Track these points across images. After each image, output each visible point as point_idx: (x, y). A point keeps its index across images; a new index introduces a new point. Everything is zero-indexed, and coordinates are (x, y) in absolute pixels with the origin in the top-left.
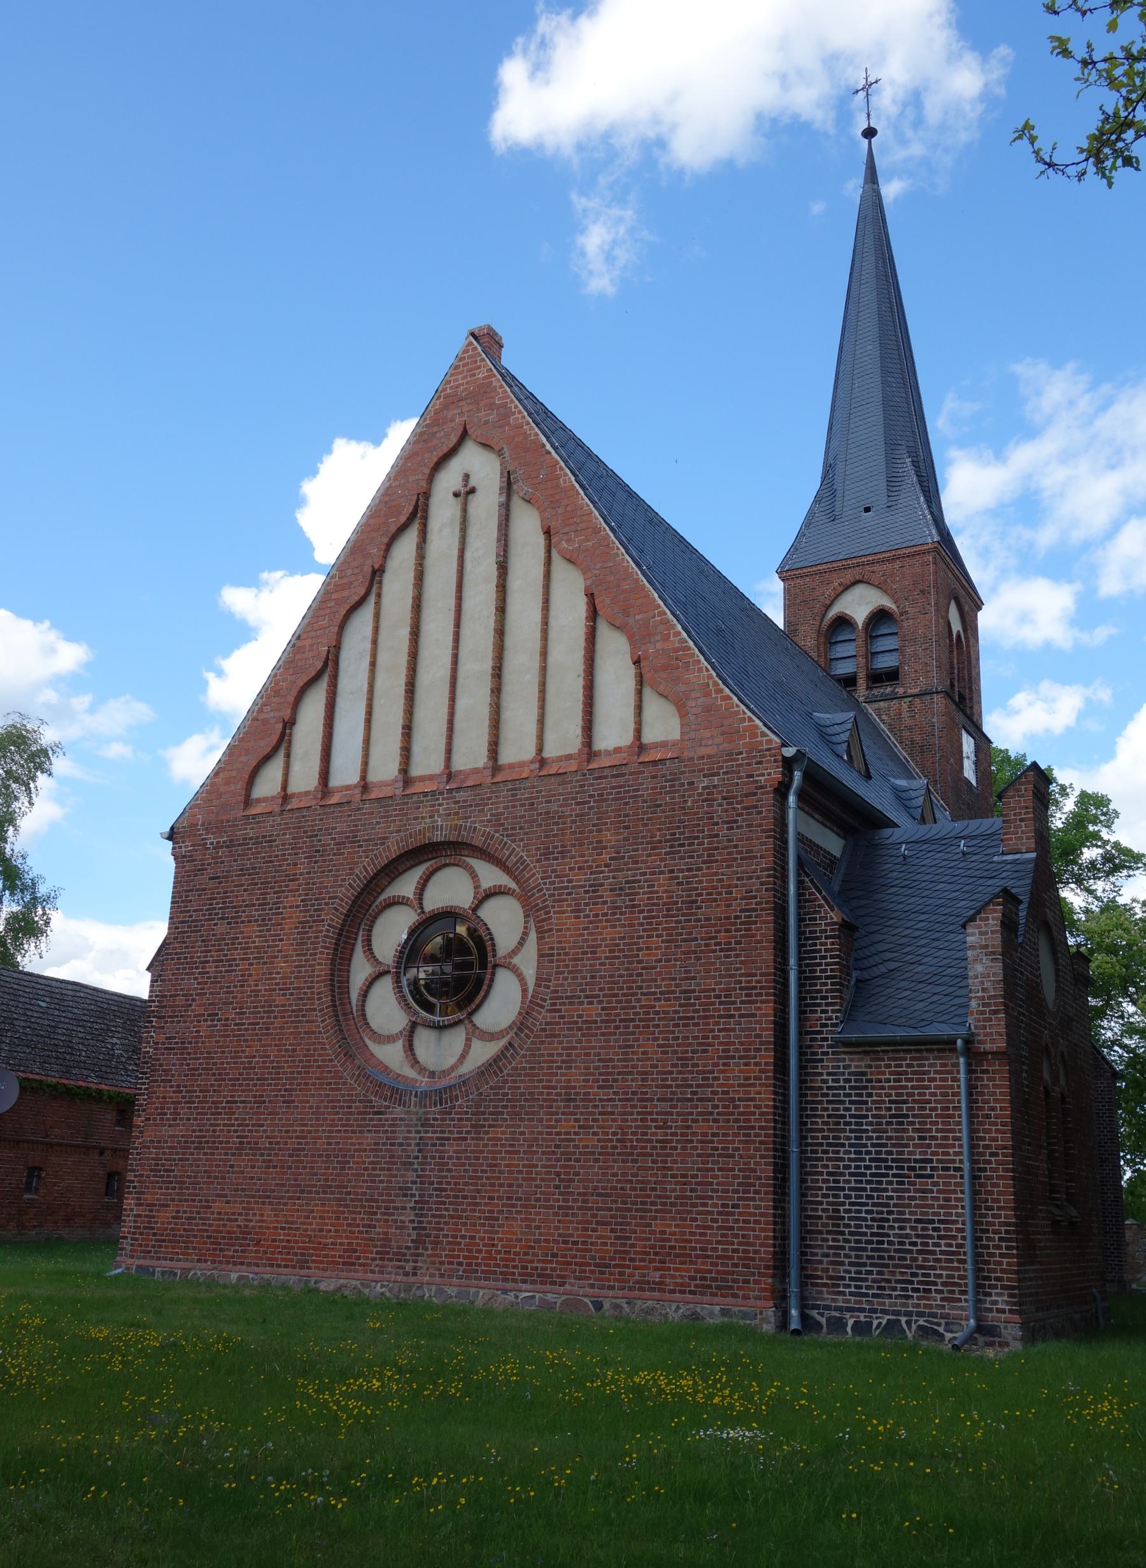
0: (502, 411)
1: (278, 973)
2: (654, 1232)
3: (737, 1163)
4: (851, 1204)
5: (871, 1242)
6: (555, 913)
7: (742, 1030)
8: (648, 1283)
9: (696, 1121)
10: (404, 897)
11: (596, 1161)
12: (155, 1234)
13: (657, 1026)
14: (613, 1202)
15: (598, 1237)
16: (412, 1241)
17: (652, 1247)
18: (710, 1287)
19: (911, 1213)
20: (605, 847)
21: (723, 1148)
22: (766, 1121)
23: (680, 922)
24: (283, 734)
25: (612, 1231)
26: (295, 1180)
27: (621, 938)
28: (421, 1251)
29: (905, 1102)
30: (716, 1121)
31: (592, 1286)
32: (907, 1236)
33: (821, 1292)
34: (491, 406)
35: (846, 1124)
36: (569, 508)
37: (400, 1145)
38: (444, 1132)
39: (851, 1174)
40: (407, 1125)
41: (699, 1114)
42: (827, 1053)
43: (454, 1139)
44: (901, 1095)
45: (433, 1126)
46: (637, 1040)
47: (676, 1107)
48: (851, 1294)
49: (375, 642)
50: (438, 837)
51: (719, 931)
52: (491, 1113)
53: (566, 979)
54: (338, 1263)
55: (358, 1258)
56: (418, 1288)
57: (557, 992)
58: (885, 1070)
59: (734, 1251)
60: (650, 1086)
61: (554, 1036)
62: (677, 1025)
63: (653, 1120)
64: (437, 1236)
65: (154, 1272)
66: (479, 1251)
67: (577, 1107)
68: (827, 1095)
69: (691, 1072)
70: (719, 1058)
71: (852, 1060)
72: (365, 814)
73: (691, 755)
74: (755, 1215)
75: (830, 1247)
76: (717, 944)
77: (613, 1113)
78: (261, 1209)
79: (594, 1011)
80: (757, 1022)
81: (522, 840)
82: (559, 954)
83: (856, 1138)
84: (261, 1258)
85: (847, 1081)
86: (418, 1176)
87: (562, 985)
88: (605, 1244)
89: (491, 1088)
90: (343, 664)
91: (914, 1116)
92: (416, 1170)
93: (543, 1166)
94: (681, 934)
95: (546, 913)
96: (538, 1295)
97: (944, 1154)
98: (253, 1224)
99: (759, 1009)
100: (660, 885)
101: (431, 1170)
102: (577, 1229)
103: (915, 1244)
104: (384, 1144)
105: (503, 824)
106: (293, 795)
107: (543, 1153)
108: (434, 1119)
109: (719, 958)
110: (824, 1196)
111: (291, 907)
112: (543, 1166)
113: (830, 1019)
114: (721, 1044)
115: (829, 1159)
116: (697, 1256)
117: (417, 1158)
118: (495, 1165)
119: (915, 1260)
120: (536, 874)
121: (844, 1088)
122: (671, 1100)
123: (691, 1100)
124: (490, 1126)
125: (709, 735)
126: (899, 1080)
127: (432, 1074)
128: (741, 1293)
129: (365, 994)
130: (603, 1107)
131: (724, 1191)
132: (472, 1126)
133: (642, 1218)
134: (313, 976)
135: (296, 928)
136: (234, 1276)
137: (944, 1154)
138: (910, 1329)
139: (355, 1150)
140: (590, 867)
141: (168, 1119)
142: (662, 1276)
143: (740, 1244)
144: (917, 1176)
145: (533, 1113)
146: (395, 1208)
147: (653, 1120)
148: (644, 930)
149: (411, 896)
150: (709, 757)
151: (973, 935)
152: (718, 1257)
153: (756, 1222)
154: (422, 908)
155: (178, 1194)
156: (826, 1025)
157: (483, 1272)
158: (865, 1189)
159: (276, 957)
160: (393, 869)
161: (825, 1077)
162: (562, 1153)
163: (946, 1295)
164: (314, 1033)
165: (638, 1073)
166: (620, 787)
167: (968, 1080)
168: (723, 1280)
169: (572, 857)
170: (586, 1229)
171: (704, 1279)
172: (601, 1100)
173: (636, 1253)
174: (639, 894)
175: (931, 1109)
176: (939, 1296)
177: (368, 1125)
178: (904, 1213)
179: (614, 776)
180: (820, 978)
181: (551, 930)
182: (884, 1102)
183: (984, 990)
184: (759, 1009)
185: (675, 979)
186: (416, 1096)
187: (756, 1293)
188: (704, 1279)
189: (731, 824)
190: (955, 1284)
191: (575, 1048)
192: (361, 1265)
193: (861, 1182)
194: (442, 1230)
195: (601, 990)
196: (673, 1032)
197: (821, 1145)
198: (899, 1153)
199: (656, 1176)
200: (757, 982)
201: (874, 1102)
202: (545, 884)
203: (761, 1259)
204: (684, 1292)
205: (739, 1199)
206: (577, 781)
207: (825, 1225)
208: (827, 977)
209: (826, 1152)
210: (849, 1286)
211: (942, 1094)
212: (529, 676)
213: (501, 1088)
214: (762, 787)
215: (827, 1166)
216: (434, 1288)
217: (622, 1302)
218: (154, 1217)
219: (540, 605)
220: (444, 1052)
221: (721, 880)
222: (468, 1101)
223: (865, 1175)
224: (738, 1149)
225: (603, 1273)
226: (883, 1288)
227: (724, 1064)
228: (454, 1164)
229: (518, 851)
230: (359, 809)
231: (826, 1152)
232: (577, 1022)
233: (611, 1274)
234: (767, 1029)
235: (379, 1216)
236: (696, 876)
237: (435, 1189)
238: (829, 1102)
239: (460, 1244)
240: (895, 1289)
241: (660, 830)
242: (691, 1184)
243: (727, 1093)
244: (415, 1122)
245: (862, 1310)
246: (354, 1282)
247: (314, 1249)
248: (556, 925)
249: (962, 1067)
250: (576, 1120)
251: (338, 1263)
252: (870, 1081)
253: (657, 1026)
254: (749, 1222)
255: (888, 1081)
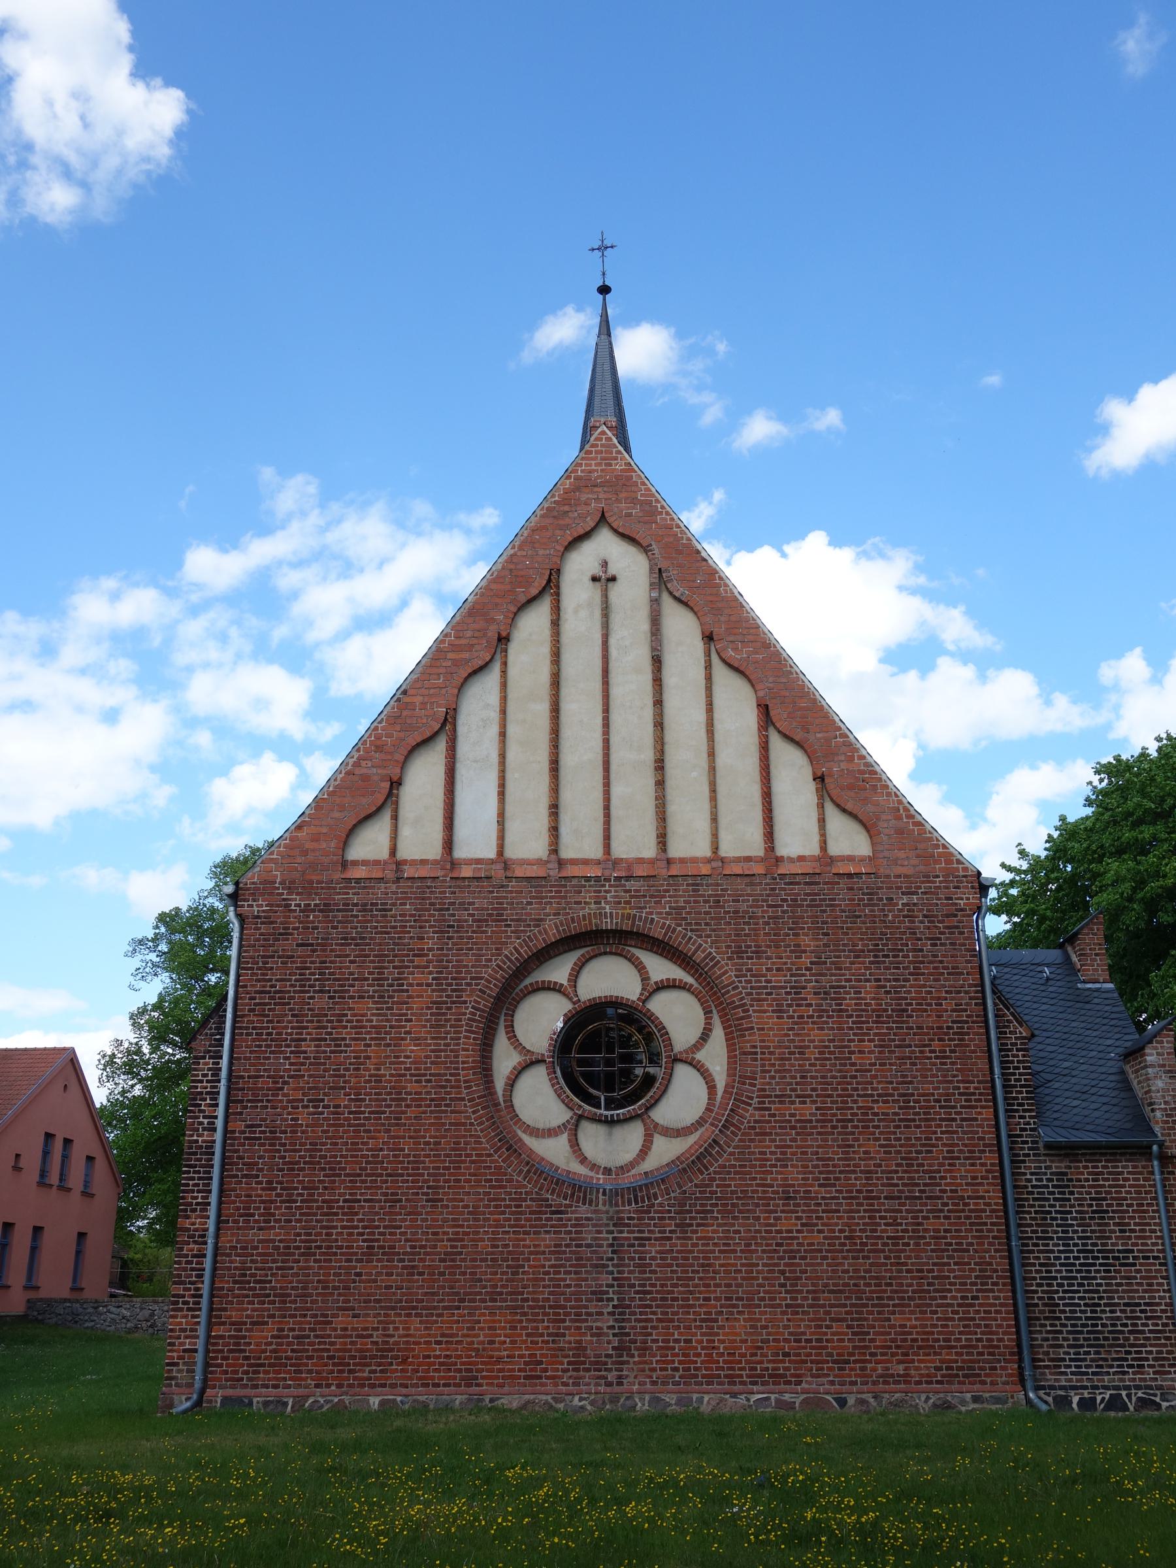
0: (647, 508)
1: (407, 1057)
2: (894, 1326)
3: (973, 1257)
4: (1065, 1292)
5: (1086, 1325)
6: (754, 1011)
7: (964, 1133)
8: (892, 1376)
9: (927, 1218)
10: (556, 983)
11: (824, 1258)
12: (247, 1358)
13: (878, 1127)
14: (847, 1298)
15: (833, 1334)
16: (614, 1348)
17: (893, 1341)
18: (957, 1376)
19: (1119, 1298)
20: (805, 951)
21: (956, 1244)
22: (997, 1217)
23: (892, 1029)
24: (390, 794)
25: (848, 1327)
26: (452, 1287)
27: (830, 1041)
28: (625, 1358)
29: (1105, 1199)
30: (946, 1218)
31: (832, 1383)
32: (1118, 1318)
33: (1044, 1374)
34: (634, 501)
35: (1052, 1219)
36: (733, 618)
37: (588, 1246)
38: (643, 1232)
39: (1061, 1265)
40: (594, 1225)
41: (928, 1211)
42: (1028, 1155)
43: (656, 1239)
44: (1100, 1193)
45: (628, 1225)
46: (857, 1140)
47: (904, 1204)
48: (1072, 1373)
49: (503, 712)
50: (607, 924)
51: (933, 1040)
52: (698, 1212)
53: (773, 1078)
54: (519, 1377)
55: (546, 1370)
56: (628, 1398)
57: (764, 1090)
58: (1083, 1171)
59: (978, 1340)
60: (876, 1185)
61: (765, 1134)
62: (899, 1127)
63: (881, 1218)
64: (645, 1342)
65: (251, 1403)
66: (699, 1355)
67: (798, 1205)
68: (1033, 1193)
69: (918, 1172)
70: (944, 1158)
71: (1052, 1161)
72: (511, 892)
73: (887, 872)
74: (995, 1305)
75: (1048, 1332)
76: (931, 1052)
77: (838, 1211)
78: (406, 1322)
79: (809, 1110)
80: (978, 1126)
81: (709, 936)
82: (763, 1053)
83: (1063, 1232)
84: (410, 1378)
85: (1049, 1180)
86: (614, 1279)
87: (769, 1084)
88: (842, 1340)
89: (696, 1186)
90: (462, 730)
91: (1113, 1212)
92: (612, 1273)
93: (764, 1265)
94: (894, 1040)
95: (744, 1011)
96: (773, 1397)
97: (1143, 1244)
98: (396, 1339)
99: (980, 1113)
100: (866, 993)
101: (630, 1272)
102: (810, 1327)
103: (1126, 1325)
104: (567, 1246)
105: (685, 919)
106: (405, 862)
107: (764, 1251)
108: (629, 1218)
109: (935, 1064)
110: (1039, 1285)
111: (418, 985)
112: (764, 1265)
113: (1029, 1123)
114: (944, 1145)
115: (1039, 1251)
116: (941, 1347)
117: (612, 1259)
118: (708, 1265)
119: (1127, 1339)
120: (727, 971)
121: (1047, 1187)
122: (899, 1198)
123: (920, 1198)
124: (698, 1225)
125: (904, 856)
126: (1097, 1180)
127: (607, 1171)
128: (988, 1380)
129: (511, 1083)
130: (826, 1205)
131: (961, 1284)
132: (676, 1225)
133: (879, 1313)
134: (457, 1062)
135: (428, 1008)
136: (375, 1402)
137: (1143, 1244)
138: (1130, 1401)
139: (531, 1253)
140: (790, 969)
141: (256, 1221)
142: (906, 1369)
143: (982, 1333)
144: (1122, 1265)
145: (748, 1211)
146: (588, 1314)
147: (881, 1218)
148: (854, 1034)
149: (565, 983)
150: (906, 876)
151: (1152, 1055)
152: (962, 1347)
153: (997, 1312)
154: (647, 998)
155: (279, 1309)
156: (1025, 1129)
157: (704, 1376)
158: (1076, 1278)
159: (403, 1039)
160: (546, 954)
161: (1028, 1177)
162: (785, 1251)
163: (1158, 1369)
164: (464, 1124)
165: (861, 1172)
166: (816, 894)
167: (1163, 1180)
168: (970, 1368)
169: (768, 958)
170: (820, 1327)
171: (951, 1368)
172: (824, 1198)
173: (876, 1347)
174: (845, 999)
175: (1128, 1205)
176: (1151, 1370)
177: (546, 1226)
178: (1113, 1298)
179: (806, 883)
180: (1015, 1086)
181: (752, 1028)
182: (1085, 1199)
183: (1166, 1103)
184: (980, 1113)
185: (892, 1083)
186: (604, 1194)
187: (1004, 1379)
188: (951, 1368)
189: (934, 940)
190: (1164, 1359)
191: (790, 1147)
192: (547, 1378)
193: (1071, 1271)
194: (651, 1334)
195: (813, 1090)
196: (895, 1133)
197: (1031, 1238)
198: (1103, 1245)
199: (891, 1271)
200: (975, 1088)
201: (1076, 1199)
202: (740, 982)
203: (1006, 1347)
204: (931, 1383)
205: (978, 1291)
206: (767, 884)
207: (1041, 1312)
208: (1022, 1086)
209: (1037, 1245)
210: (1070, 1367)
211: (1136, 1192)
212: (694, 774)
213: (707, 1186)
214: (962, 910)
215: (1039, 1258)
216: (647, 1397)
217: (869, 1397)
218: (244, 1337)
219: (704, 707)
220: (612, 1147)
221: (930, 993)
222: (670, 1199)
223: (1074, 1265)
224: (972, 1244)
225: (843, 1369)
226: (1101, 1367)
227: (950, 1165)
228: (658, 1265)
229: (703, 947)
230: (502, 886)
231: (1037, 1245)
232: (790, 1121)
233: (851, 1369)
234: (990, 1133)
235: (567, 1324)
236: (904, 986)
237: (637, 1292)
238: (1034, 1199)
239: (674, 1348)
240: (1112, 1366)
241: (862, 939)
242: (928, 1278)
243: (956, 1191)
244: (605, 1221)
245: (1086, 1388)
246: (544, 1397)
247: (483, 1363)
248: (757, 1023)
249: (1157, 1170)
250: (797, 1218)
251: (519, 1377)
252: (1071, 1180)
253: (878, 1127)
254: (989, 1312)
255: (1087, 1180)
